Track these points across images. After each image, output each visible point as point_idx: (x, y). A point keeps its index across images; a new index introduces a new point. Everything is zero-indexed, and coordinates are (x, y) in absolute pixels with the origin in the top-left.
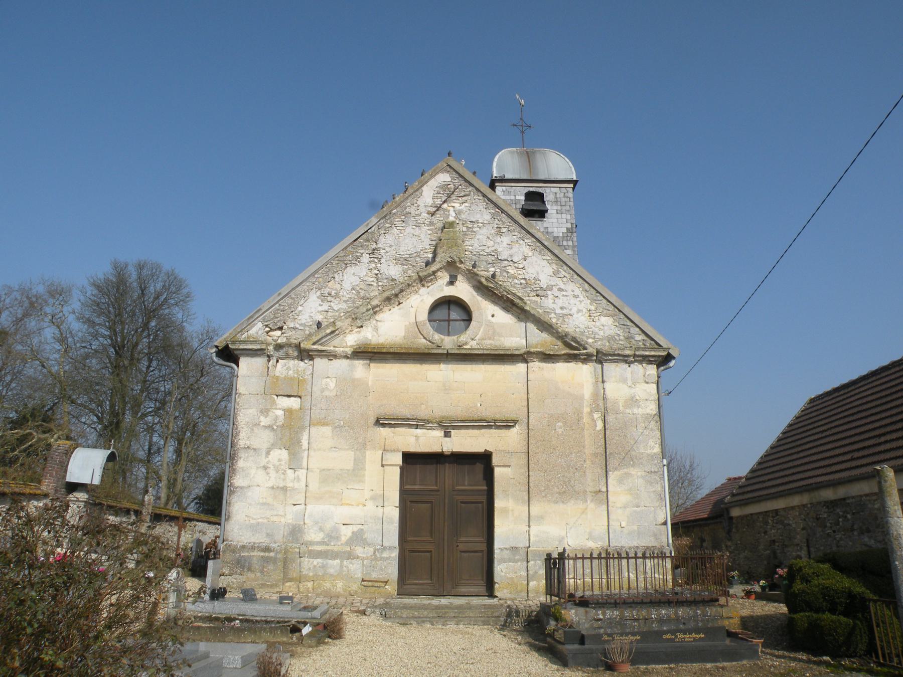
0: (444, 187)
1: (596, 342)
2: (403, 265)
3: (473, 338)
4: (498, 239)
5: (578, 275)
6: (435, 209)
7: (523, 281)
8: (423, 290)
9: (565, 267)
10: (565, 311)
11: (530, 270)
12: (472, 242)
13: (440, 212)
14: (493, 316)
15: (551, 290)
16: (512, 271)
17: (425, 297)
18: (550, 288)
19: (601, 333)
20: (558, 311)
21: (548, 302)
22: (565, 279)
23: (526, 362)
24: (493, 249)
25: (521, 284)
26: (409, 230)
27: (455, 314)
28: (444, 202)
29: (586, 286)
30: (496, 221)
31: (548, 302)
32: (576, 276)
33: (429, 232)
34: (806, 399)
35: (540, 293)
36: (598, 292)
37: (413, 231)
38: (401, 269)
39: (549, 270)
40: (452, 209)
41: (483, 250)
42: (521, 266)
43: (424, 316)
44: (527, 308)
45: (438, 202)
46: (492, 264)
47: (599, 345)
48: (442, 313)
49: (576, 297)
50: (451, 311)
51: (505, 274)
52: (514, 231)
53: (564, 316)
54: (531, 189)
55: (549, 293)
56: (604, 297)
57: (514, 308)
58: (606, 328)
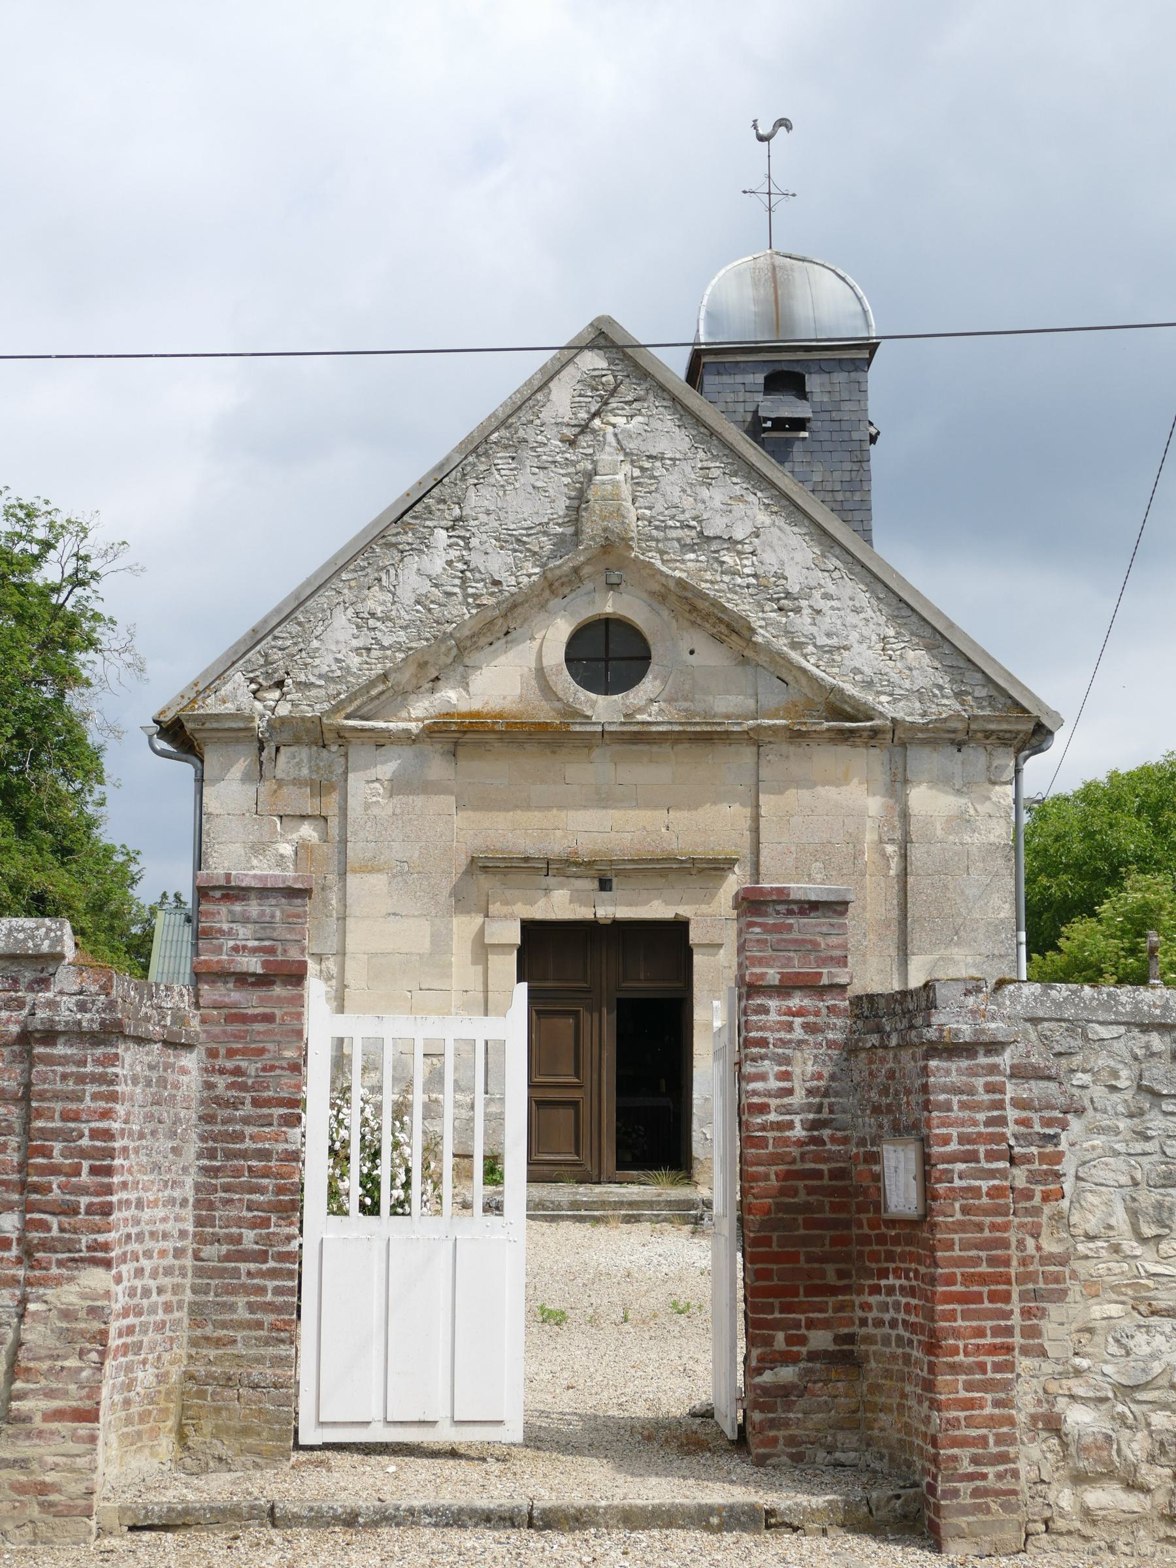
0: (592, 382)
1: (896, 701)
4: (704, 493)
5: (863, 566)
7: (753, 581)
9: (837, 550)
10: (834, 641)
11: (768, 557)
14: (692, 652)
15: (808, 597)
16: (729, 559)
18: (807, 591)
20: (822, 640)
21: (802, 623)
22: (836, 574)
26: (525, 478)
30: (701, 454)
31: (802, 623)
33: (567, 480)
35: (787, 602)
37: (532, 479)
40: (610, 429)
42: (748, 548)
43: (555, 655)
46: (692, 548)
49: (856, 611)
50: (608, 653)
51: (716, 566)
53: (832, 650)
54: (779, 367)
55: (804, 603)
56: (913, 609)
57: (734, 637)
58: (915, 673)
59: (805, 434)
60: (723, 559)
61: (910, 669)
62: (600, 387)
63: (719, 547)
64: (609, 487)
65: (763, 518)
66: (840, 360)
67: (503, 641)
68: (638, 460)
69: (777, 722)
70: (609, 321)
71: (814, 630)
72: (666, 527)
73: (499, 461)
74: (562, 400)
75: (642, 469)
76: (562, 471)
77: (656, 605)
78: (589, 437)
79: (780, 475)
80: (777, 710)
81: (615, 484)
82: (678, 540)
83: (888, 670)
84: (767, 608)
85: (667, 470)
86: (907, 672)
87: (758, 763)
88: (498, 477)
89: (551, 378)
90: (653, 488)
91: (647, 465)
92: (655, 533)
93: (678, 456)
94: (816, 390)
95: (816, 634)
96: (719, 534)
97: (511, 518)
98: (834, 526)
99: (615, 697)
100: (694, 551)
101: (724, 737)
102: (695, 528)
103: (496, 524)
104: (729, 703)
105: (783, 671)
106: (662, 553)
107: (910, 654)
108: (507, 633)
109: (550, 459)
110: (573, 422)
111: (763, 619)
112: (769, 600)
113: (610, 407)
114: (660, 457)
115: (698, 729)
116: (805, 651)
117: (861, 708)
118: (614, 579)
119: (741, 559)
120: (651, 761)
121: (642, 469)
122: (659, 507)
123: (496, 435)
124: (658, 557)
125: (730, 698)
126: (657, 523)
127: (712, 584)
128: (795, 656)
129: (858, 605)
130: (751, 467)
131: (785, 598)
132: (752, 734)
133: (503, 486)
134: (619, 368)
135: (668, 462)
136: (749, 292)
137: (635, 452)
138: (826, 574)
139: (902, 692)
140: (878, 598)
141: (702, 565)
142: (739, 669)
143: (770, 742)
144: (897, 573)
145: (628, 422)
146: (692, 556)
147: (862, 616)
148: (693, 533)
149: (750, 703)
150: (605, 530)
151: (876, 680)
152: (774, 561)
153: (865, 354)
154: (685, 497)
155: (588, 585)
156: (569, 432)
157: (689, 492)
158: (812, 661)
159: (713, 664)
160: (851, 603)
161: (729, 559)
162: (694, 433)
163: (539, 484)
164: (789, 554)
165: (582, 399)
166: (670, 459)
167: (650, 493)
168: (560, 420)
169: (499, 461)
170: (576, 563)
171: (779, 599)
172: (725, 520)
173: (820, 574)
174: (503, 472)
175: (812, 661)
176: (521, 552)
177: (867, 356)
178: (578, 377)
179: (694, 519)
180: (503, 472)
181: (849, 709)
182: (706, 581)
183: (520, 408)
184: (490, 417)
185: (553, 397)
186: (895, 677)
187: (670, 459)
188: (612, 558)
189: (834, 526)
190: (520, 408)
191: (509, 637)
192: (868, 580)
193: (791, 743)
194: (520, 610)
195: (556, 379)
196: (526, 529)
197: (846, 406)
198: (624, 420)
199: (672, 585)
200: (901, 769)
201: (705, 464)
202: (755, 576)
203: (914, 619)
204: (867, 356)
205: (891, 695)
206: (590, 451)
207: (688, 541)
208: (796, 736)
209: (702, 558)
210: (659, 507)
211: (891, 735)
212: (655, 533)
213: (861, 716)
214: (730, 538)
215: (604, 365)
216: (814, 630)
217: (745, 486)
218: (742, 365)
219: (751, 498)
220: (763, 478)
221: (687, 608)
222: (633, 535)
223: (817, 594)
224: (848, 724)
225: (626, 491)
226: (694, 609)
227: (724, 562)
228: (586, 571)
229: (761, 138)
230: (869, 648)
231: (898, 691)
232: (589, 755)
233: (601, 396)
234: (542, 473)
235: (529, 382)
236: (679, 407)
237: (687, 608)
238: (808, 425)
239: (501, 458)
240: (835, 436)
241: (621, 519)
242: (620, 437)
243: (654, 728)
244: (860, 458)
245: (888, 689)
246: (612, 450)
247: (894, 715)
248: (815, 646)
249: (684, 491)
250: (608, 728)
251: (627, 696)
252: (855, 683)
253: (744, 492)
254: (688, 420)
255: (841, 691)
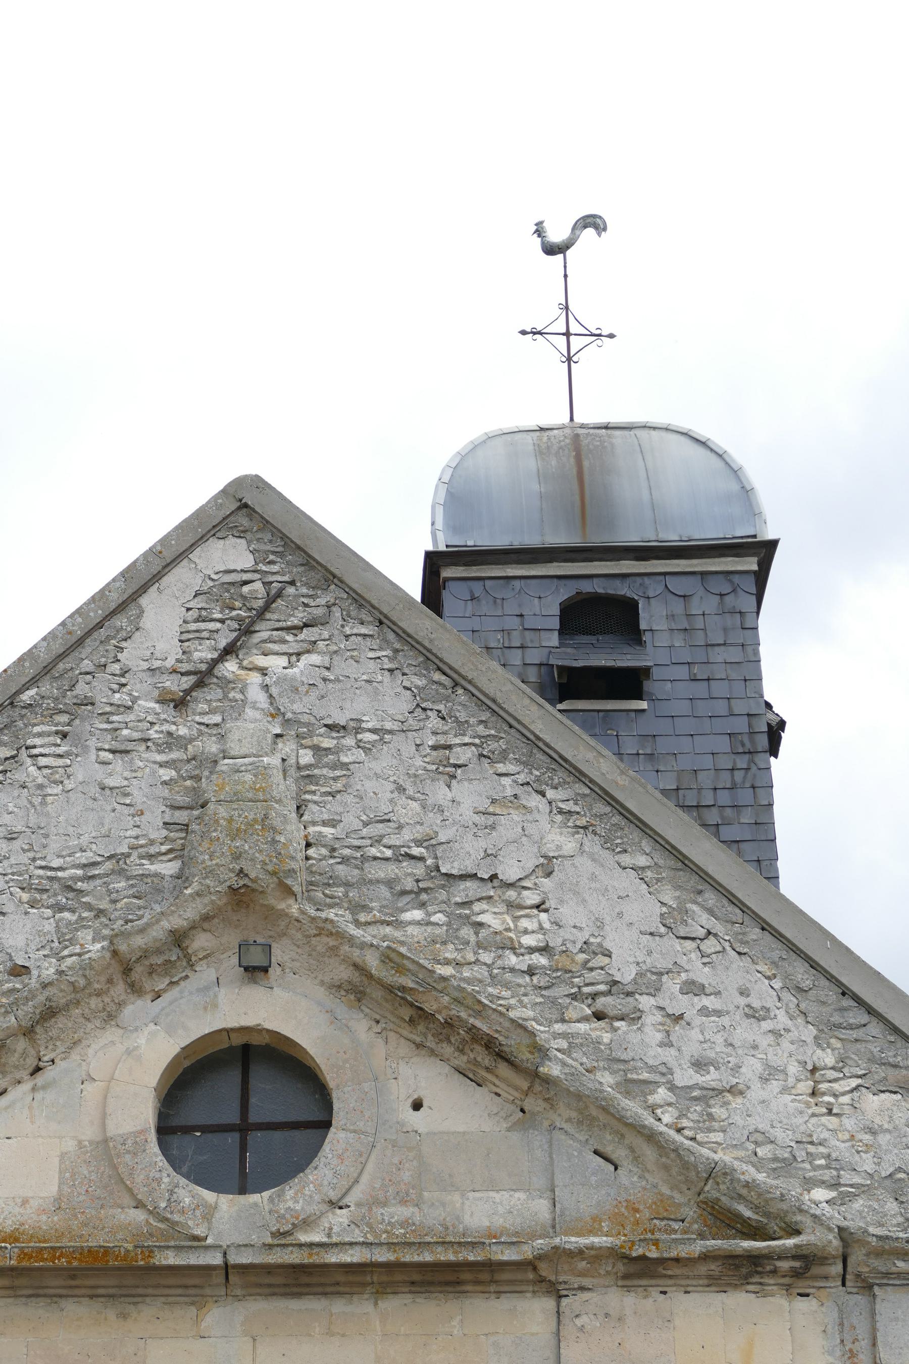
0: (227, 590)
1: (843, 1199)
2: (59, 908)
3: (332, 1199)
4: (440, 793)
5: (765, 927)
6: (187, 682)
7: (541, 960)
8: (136, 1009)
9: (711, 898)
10: (711, 1078)
11: (569, 913)
12: (334, 806)
13: (213, 693)
14: (417, 1106)
15: (655, 990)
16: (493, 918)
17: (141, 1039)
18: (651, 981)
19: (867, 1163)
20: (685, 1077)
21: (645, 1041)
22: (710, 945)
23: (556, 1291)
24: (419, 832)
25: (531, 972)
26: (86, 769)
27: (272, 1098)
28: (229, 651)
29: (802, 974)
30: (434, 722)
31: (645, 1041)
32: (755, 933)
33: (167, 774)
34: (253, 472)
35: (610, 1002)
36: (845, 992)
37: (100, 773)
38: (49, 926)
39: (645, 908)
40: (255, 678)
41: (377, 840)
42: (531, 898)
43: (138, 1113)
44: (553, 1070)
45: (204, 653)
46: (418, 895)
47: (858, 1215)
48: (217, 1101)
49: (755, 1015)
50: (243, 1104)
51: (467, 932)
52: (503, 757)
53: (710, 1095)
54: (587, 587)
55: (645, 1002)
56: (871, 1011)
57: (503, 1069)
58: (883, 1139)
59: (643, 705)
60: (479, 919)
61: (873, 1132)
62: (238, 604)
63: (472, 895)
64: (248, 777)
65: (559, 840)
66: (703, 574)
67: (26, 1086)
68: (311, 734)
69: (596, 1240)
70: (257, 483)
71: (668, 1055)
72: (365, 859)
73: (37, 741)
74: (162, 630)
75: (316, 749)
76: (160, 758)
77: (342, 1011)
78: (216, 693)
79: (590, 755)
80: (596, 1219)
81: (262, 772)
82: (390, 883)
83: (825, 1135)
84: (571, 1014)
85: (367, 751)
86: (867, 1138)
87: (558, 1333)
88: (32, 769)
89: (143, 589)
90: (339, 785)
91: (327, 743)
92: (341, 870)
93: (388, 725)
94: (661, 625)
95: (672, 1063)
96: (471, 870)
97: (55, 844)
98: (704, 850)
99: (254, 1198)
100: (422, 905)
101: (485, 1276)
102: (421, 859)
103: (24, 858)
104: (495, 1207)
105: (609, 1128)
106: (357, 908)
107: (873, 1103)
108: (38, 1069)
109: (136, 735)
110: (185, 667)
111: (564, 1035)
112: (574, 997)
113: (256, 638)
114: (354, 728)
115: (428, 1257)
116: (651, 1099)
117: (774, 1208)
118: (257, 959)
119: (516, 919)
120: (330, 1333)
121: (316, 749)
122: (351, 821)
123: (32, 692)
124: (349, 917)
125: (497, 1196)
126: (347, 852)
127: (462, 968)
128: (631, 1107)
129: (756, 1004)
130: (534, 742)
131: (609, 993)
132: (545, 1270)
133: (41, 787)
134: (275, 568)
135: (368, 737)
136: (531, 464)
137: (305, 718)
138: (689, 945)
139: (857, 1180)
140: (800, 990)
141: (438, 931)
142: (515, 1136)
143: (582, 1289)
144: (833, 939)
145: (291, 665)
146: (417, 914)
147: (766, 1025)
148: (419, 870)
149: (541, 1208)
150: (237, 857)
151: (801, 1155)
152: (583, 922)
153: (751, 564)
154: (403, 800)
155: (206, 974)
156: (176, 685)
157: (410, 791)
158: (666, 1119)
159: (461, 1129)
160: (742, 1001)
161: (493, 918)
162: (421, 682)
163: (111, 782)
164: (609, 905)
165: (202, 626)
166: (373, 731)
167: (332, 795)
168: (157, 664)
169: (37, 741)
170: (177, 922)
171: (594, 996)
172: (482, 844)
173: (677, 945)
174: (43, 761)
175: (666, 1119)
176: (73, 911)
177: (755, 567)
178: (197, 583)
179: (419, 843)
180: (43, 761)
181: (748, 1213)
182: (447, 962)
183: (80, 642)
184: (21, 659)
185: (147, 622)
186: (840, 1148)
187: (373, 731)
188: (251, 914)
189: (704, 850)
190: (80, 642)
191: (40, 1079)
192: (776, 955)
193: (628, 1288)
194: (61, 1021)
195: (153, 590)
196: (84, 866)
197: (719, 655)
198: (283, 661)
199: (372, 962)
200: (865, 1344)
201: (442, 740)
202: (545, 950)
203: (875, 1029)
204: (755, 567)
205: (835, 1186)
206: (217, 719)
207: (409, 884)
208: (640, 1270)
209: (439, 918)
210: (351, 821)
211: (839, 1268)
212: (341, 870)
213: (773, 1226)
214: (494, 877)
215: (248, 561)
216: (668, 1055)
217: (521, 778)
218: (517, 583)
219: (534, 801)
220: (561, 762)
221: (407, 1013)
222: (294, 865)
223: (672, 985)
224: (747, 1244)
225: (283, 787)
226: (420, 1016)
227: (481, 925)
228: (200, 942)
229: (551, 250)
230: (785, 1090)
231: (847, 1177)
232: (197, 1321)
233: (239, 619)
234: (119, 764)
235: (101, 595)
236: (391, 636)
237: (407, 1013)
238: (647, 686)
239: (40, 735)
240: (702, 708)
241: (269, 836)
242: (274, 691)
243: (333, 1258)
244: (748, 745)
245: (827, 1175)
246: (258, 715)
247: (845, 1224)
248: (672, 1088)
249: (401, 789)
250: (233, 1259)
251: (283, 1191)
252: (759, 1163)
253: (519, 790)
254: (409, 659)
255: (728, 1173)
